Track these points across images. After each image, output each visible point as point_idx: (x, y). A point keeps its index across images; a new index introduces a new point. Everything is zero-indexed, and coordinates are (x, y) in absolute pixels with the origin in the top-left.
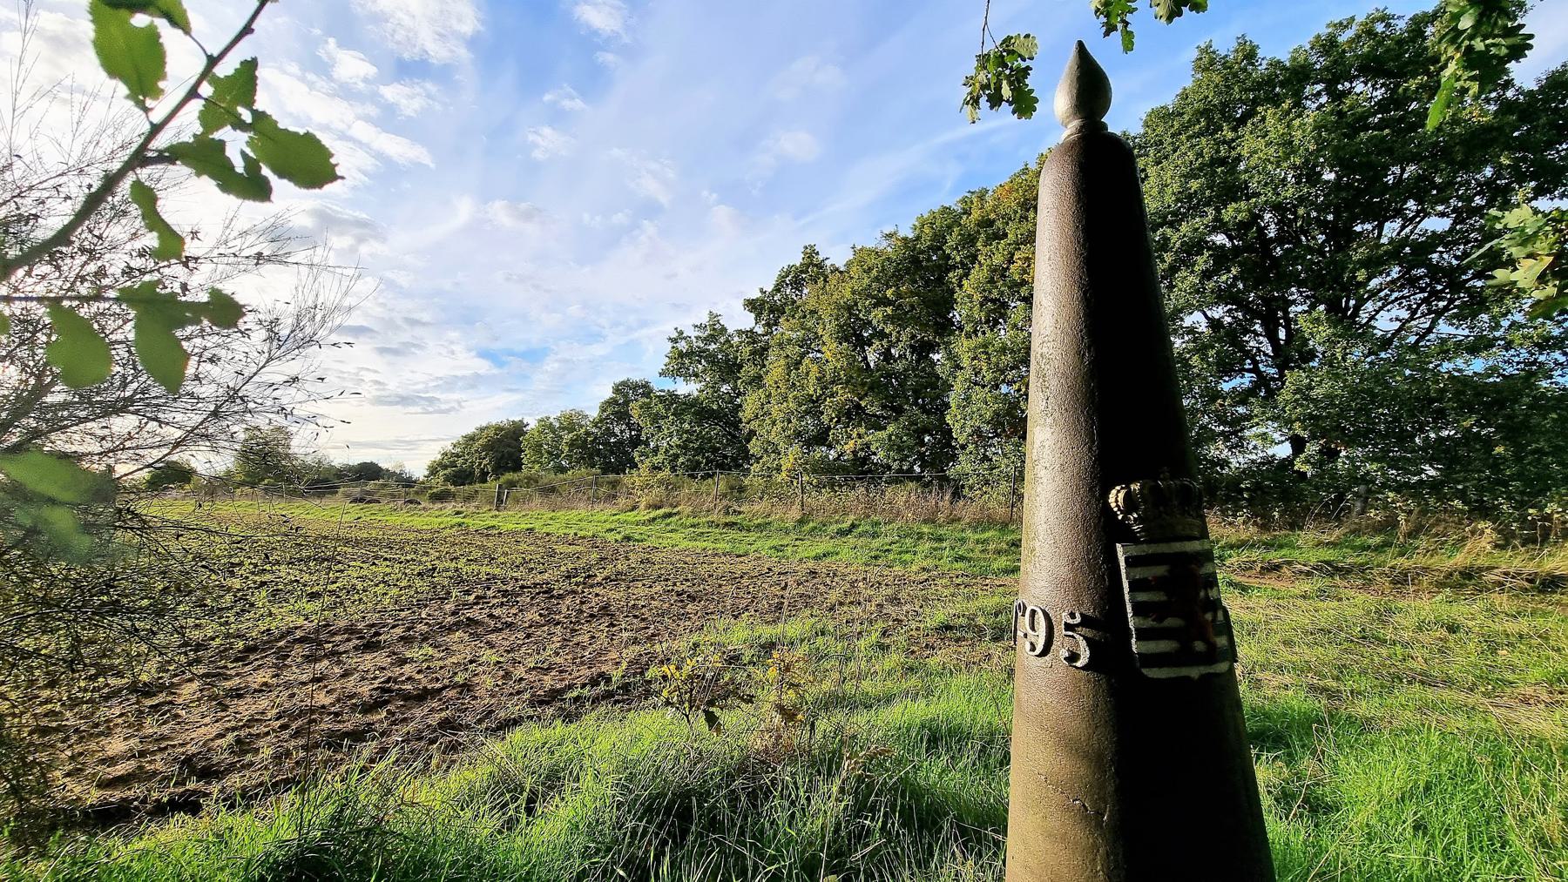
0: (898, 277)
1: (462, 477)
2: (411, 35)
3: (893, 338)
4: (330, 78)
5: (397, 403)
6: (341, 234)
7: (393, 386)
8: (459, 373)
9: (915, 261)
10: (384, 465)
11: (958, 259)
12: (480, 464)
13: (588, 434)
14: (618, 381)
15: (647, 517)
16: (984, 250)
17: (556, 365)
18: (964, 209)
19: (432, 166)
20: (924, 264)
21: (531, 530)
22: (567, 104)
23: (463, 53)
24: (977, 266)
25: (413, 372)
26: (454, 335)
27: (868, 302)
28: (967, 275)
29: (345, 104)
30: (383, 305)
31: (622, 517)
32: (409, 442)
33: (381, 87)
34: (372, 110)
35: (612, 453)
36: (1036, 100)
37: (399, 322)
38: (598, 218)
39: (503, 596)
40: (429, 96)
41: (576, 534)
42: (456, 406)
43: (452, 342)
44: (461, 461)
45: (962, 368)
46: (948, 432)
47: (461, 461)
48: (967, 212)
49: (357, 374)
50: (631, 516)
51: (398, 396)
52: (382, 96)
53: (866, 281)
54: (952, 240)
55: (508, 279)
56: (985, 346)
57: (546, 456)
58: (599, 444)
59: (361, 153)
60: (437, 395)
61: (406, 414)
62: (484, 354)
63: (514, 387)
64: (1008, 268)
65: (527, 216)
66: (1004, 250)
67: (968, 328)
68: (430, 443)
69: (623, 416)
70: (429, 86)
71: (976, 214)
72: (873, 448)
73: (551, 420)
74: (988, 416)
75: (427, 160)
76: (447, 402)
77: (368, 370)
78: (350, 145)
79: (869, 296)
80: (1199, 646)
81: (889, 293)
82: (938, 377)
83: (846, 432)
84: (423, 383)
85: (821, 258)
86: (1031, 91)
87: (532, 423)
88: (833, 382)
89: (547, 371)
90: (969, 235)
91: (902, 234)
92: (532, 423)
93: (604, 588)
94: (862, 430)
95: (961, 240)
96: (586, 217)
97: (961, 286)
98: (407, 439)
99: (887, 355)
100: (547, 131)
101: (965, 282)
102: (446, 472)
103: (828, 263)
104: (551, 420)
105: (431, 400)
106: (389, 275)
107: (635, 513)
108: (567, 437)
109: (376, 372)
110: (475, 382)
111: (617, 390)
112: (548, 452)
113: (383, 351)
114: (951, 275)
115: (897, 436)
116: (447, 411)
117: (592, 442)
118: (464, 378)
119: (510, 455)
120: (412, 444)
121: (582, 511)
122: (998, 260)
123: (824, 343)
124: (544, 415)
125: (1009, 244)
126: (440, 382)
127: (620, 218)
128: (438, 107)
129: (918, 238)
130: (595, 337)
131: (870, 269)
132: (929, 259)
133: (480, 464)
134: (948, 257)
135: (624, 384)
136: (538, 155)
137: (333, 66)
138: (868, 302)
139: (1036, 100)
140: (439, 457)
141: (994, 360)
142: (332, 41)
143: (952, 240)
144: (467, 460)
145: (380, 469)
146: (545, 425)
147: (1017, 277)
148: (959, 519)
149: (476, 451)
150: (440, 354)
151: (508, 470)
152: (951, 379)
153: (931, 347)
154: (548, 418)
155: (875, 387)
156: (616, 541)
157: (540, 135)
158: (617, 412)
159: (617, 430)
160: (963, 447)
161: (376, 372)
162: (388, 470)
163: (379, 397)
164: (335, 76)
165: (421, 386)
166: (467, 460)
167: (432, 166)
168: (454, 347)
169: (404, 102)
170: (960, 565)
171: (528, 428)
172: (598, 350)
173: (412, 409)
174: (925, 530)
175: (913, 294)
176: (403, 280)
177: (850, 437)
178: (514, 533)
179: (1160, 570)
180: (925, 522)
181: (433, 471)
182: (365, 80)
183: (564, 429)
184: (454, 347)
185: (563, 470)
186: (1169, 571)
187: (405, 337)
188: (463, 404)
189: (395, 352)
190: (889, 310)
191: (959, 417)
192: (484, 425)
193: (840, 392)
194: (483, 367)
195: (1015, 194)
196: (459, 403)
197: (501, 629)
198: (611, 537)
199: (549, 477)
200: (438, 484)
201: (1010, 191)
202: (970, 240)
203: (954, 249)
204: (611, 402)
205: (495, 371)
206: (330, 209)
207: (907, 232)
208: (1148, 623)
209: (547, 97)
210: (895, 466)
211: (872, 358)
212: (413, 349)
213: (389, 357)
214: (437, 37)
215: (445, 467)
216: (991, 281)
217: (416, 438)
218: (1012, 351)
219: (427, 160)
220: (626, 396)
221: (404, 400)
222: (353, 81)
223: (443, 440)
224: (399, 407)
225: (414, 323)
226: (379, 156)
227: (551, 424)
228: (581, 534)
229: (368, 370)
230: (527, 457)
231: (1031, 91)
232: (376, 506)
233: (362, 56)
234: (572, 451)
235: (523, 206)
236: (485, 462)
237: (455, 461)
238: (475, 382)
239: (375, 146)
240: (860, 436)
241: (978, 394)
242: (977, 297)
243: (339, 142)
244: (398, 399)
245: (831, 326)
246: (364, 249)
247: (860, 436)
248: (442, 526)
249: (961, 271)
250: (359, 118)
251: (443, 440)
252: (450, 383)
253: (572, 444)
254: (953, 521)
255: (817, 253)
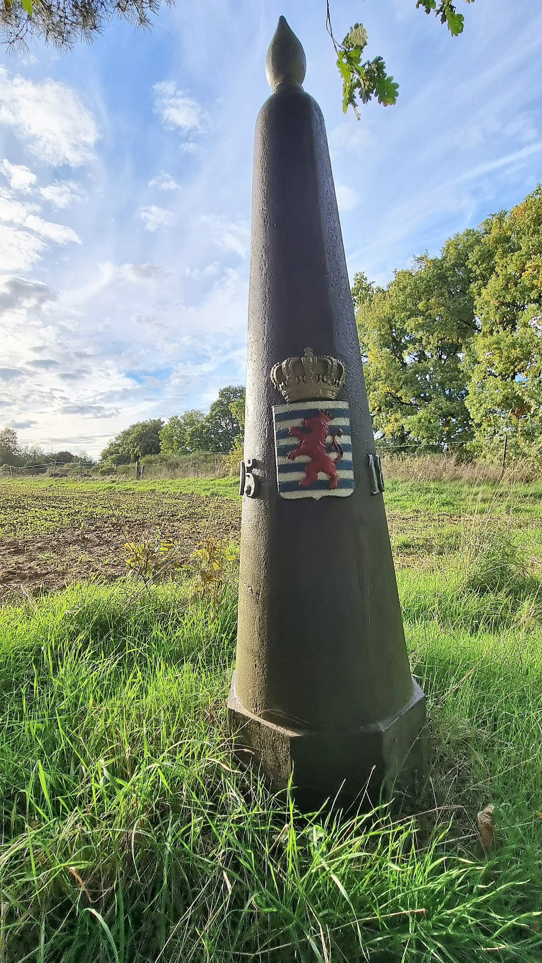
0: (428, 291)
1: (122, 460)
2: (55, 148)
3: (424, 343)
4: (9, 187)
5: (77, 412)
6: (29, 297)
7: (73, 400)
8: (115, 389)
9: (442, 278)
10: (74, 453)
11: (478, 272)
12: (133, 451)
13: (203, 427)
14: (223, 387)
15: (233, 481)
16: (501, 262)
17: (178, 380)
18: (485, 229)
19: (80, 242)
20: (450, 279)
21: (153, 491)
22: (165, 186)
23: (92, 157)
24: (494, 276)
25: (85, 390)
26: (109, 363)
27: (403, 314)
28: (485, 285)
29: (19, 204)
30: (60, 344)
31: (217, 482)
32: (88, 438)
33: (41, 189)
34: (37, 208)
35: (220, 440)
36: (397, 86)
37: (73, 356)
38: (196, 271)
39: (113, 526)
40: (72, 192)
41: (181, 493)
42: (114, 411)
43: (107, 368)
44: (121, 449)
45: (479, 363)
46: (467, 416)
47: (121, 449)
48: (488, 232)
49: (51, 393)
50: (223, 481)
51: (77, 407)
52: (42, 195)
53: (402, 298)
54: (473, 257)
55: (139, 320)
56: (498, 343)
57: (176, 443)
58: (211, 434)
59: (33, 238)
60: (102, 405)
61: (83, 419)
62: (130, 375)
63: (149, 397)
64: (521, 276)
65: (147, 273)
66: (516, 260)
67: (486, 329)
68: (101, 438)
69: (226, 413)
70: (73, 185)
71: (495, 232)
72: (406, 429)
73: (179, 418)
74: (499, 398)
75: (76, 238)
76: (110, 409)
77: (57, 390)
78: (27, 233)
79: (404, 309)
80: (322, 476)
81: (421, 306)
82: (460, 372)
83: (387, 417)
84: (93, 397)
85: (368, 282)
86: (390, 79)
87: (166, 421)
88: (376, 380)
89: (172, 385)
90: (489, 251)
91: (431, 257)
92: (166, 421)
93: (180, 522)
94: (398, 415)
95: (481, 256)
96: (188, 271)
97: (480, 294)
98: (87, 436)
99: (422, 356)
100: (154, 209)
101: (483, 291)
102: (113, 457)
103: (374, 286)
104: (179, 418)
105: (99, 409)
106: (62, 323)
107: (226, 478)
108: (189, 430)
109: (62, 391)
110: (125, 395)
111: (222, 394)
112: (177, 441)
113: (64, 376)
114: (472, 286)
115: (425, 418)
116: (110, 416)
117: (207, 432)
118: (117, 392)
119: (153, 443)
120: (88, 439)
121: (191, 478)
122: (511, 270)
123: (369, 350)
124: (173, 416)
125: (522, 255)
126: (103, 396)
127: (211, 269)
128: (79, 199)
129: (444, 259)
130: (201, 359)
131: (405, 287)
132: (454, 275)
133: (133, 451)
134: (471, 271)
135: (227, 390)
136: (150, 227)
137: (10, 178)
138: (403, 314)
139: (397, 86)
140: (108, 447)
141: (505, 353)
142: (6, 161)
143: (473, 257)
144: (125, 448)
145: (72, 456)
146: (175, 422)
147: (527, 283)
148: (460, 478)
149: (131, 442)
150: (101, 376)
151: (150, 452)
152: (470, 372)
153: (457, 348)
154: (176, 417)
155: (409, 382)
156: (207, 497)
157: (150, 212)
158: (222, 411)
159: (223, 424)
160: (479, 425)
161: (62, 391)
162: (77, 457)
163: (66, 408)
164: (12, 185)
165: (91, 400)
166: (125, 448)
167: (80, 242)
168: (109, 371)
169: (56, 199)
170: (446, 508)
171: (164, 425)
172: (206, 368)
173: (87, 415)
174: (432, 486)
175: (440, 305)
176: (71, 326)
177: (389, 421)
178: (142, 493)
179: (297, 422)
180: (434, 480)
181: (104, 457)
182: (31, 186)
183: (187, 424)
184: (109, 371)
185: (186, 452)
186: (303, 423)
187: (78, 365)
188: (119, 410)
189: (72, 377)
190: (420, 319)
191: (475, 402)
192: (135, 424)
193: (381, 387)
194: (129, 383)
195: (529, 212)
196: (117, 410)
197: (103, 545)
198: (203, 494)
199: (176, 457)
200: (108, 464)
201: (525, 210)
202: (487, 256)
203: (475, 264)
204: (219, 404)
205: (138, 387)
206: (19, 280)
207: (437, 254)
208: (286, 461)
209: (151, 183)
210: (424, 442)
211: (408, 359)
212: (83, 374)
213: (68, 381)
214: (72, 147)
215: (112, 454)
216: (506, 288)
217: (92, 435)
218: (521, 346)
219: (76, 238)
220: (228, 398)
221: (82, 409)
222: (23, 187)
223: (109, 435)
224: (79, 414)
225: (82, 356)
226: (47, 240)
227: (179, 421)
228: (184, 492)
229: (57, 390)
230: (163, 444)
231: (390, 79)
232: (64, 478)
233: (29, 170)
234: (193, 440)
235: (144, 266)
236: (137, 449)
237: (117, 450)
238: (125, 395)
239: (43, 232)
240: (396, 420)
241: (491, 382)
242: (494, 303)
243: (19, 232)
244: (77, 409)
245: (375, 335)
246: (45, 307)
247: (396, 420)
248: (100, 489)
249: (480, 282)
250: (29, 213)
251: (109, 435)
252: (110, 397)
253: (192, 435)
254: (455, 479)
255: (366, 279)
